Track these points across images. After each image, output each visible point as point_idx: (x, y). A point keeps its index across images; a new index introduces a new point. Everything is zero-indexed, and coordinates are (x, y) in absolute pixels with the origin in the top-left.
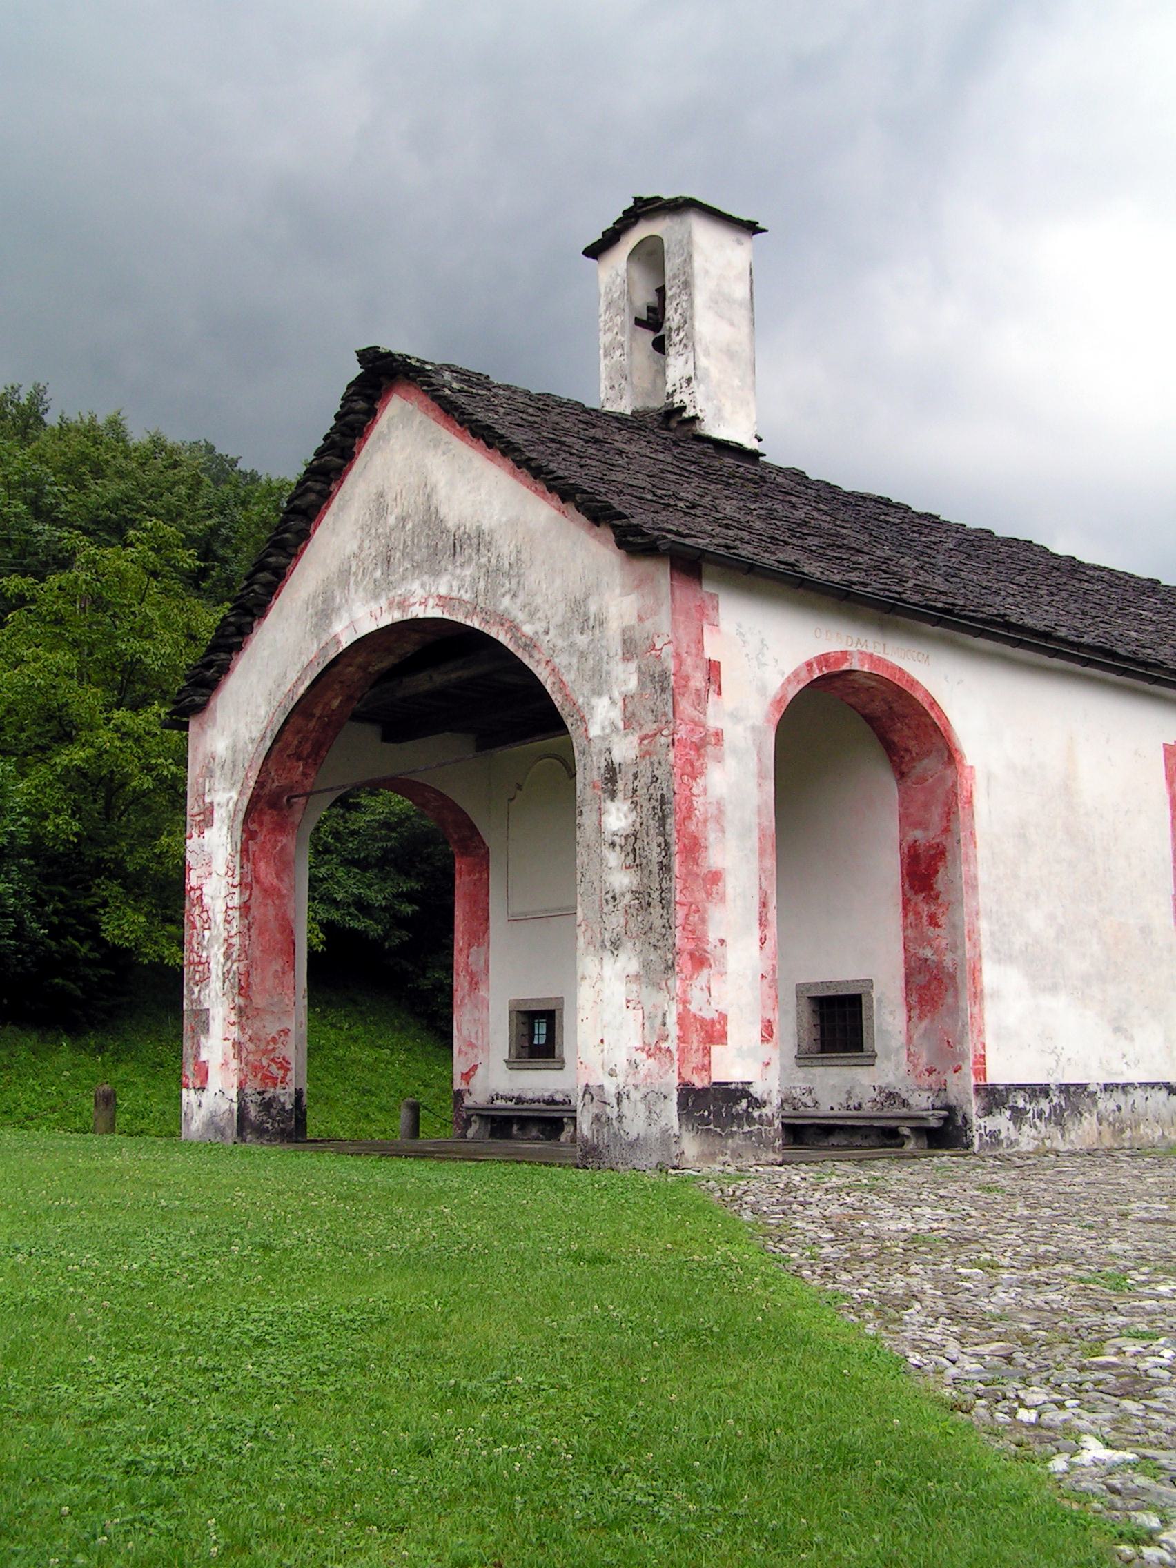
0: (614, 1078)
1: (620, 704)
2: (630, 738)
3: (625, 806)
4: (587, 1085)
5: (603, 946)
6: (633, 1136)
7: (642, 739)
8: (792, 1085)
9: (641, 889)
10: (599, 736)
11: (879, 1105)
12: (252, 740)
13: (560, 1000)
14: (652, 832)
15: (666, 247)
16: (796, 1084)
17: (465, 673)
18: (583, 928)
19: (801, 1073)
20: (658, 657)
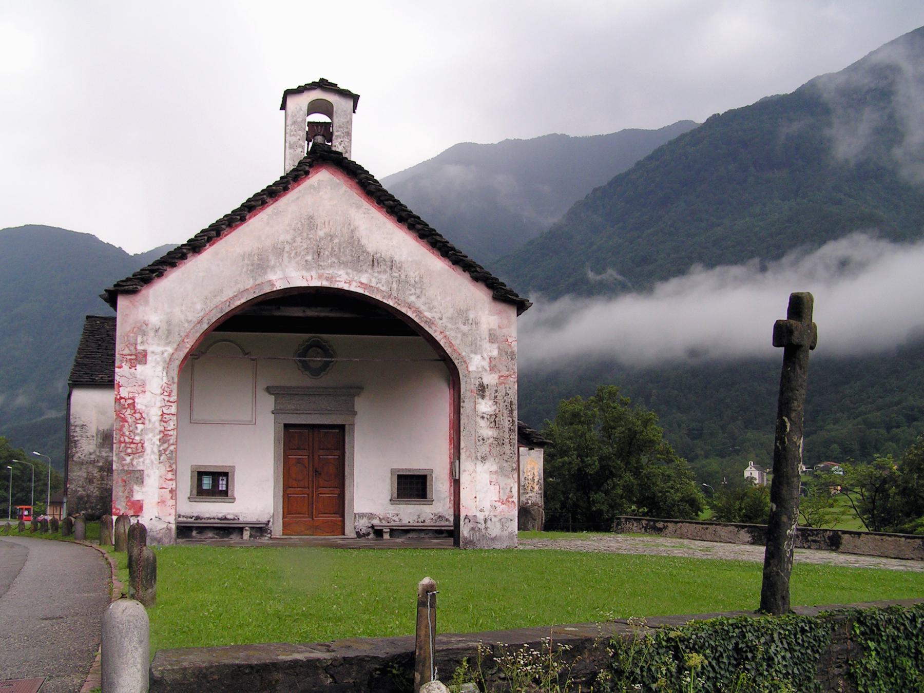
0: (483, 513)
1: (488, 360)
2: (493, 375)
3: (491, 403)
5: (477, 458)
6: (493, 535)
7: (500, 377)
10: (475, 371)
12: (189, 322)
13: (233, 467)
14: (505, 415)
15: (335, 109)
17: (322, 314)
18: (464, 450)
19: (392, 507)
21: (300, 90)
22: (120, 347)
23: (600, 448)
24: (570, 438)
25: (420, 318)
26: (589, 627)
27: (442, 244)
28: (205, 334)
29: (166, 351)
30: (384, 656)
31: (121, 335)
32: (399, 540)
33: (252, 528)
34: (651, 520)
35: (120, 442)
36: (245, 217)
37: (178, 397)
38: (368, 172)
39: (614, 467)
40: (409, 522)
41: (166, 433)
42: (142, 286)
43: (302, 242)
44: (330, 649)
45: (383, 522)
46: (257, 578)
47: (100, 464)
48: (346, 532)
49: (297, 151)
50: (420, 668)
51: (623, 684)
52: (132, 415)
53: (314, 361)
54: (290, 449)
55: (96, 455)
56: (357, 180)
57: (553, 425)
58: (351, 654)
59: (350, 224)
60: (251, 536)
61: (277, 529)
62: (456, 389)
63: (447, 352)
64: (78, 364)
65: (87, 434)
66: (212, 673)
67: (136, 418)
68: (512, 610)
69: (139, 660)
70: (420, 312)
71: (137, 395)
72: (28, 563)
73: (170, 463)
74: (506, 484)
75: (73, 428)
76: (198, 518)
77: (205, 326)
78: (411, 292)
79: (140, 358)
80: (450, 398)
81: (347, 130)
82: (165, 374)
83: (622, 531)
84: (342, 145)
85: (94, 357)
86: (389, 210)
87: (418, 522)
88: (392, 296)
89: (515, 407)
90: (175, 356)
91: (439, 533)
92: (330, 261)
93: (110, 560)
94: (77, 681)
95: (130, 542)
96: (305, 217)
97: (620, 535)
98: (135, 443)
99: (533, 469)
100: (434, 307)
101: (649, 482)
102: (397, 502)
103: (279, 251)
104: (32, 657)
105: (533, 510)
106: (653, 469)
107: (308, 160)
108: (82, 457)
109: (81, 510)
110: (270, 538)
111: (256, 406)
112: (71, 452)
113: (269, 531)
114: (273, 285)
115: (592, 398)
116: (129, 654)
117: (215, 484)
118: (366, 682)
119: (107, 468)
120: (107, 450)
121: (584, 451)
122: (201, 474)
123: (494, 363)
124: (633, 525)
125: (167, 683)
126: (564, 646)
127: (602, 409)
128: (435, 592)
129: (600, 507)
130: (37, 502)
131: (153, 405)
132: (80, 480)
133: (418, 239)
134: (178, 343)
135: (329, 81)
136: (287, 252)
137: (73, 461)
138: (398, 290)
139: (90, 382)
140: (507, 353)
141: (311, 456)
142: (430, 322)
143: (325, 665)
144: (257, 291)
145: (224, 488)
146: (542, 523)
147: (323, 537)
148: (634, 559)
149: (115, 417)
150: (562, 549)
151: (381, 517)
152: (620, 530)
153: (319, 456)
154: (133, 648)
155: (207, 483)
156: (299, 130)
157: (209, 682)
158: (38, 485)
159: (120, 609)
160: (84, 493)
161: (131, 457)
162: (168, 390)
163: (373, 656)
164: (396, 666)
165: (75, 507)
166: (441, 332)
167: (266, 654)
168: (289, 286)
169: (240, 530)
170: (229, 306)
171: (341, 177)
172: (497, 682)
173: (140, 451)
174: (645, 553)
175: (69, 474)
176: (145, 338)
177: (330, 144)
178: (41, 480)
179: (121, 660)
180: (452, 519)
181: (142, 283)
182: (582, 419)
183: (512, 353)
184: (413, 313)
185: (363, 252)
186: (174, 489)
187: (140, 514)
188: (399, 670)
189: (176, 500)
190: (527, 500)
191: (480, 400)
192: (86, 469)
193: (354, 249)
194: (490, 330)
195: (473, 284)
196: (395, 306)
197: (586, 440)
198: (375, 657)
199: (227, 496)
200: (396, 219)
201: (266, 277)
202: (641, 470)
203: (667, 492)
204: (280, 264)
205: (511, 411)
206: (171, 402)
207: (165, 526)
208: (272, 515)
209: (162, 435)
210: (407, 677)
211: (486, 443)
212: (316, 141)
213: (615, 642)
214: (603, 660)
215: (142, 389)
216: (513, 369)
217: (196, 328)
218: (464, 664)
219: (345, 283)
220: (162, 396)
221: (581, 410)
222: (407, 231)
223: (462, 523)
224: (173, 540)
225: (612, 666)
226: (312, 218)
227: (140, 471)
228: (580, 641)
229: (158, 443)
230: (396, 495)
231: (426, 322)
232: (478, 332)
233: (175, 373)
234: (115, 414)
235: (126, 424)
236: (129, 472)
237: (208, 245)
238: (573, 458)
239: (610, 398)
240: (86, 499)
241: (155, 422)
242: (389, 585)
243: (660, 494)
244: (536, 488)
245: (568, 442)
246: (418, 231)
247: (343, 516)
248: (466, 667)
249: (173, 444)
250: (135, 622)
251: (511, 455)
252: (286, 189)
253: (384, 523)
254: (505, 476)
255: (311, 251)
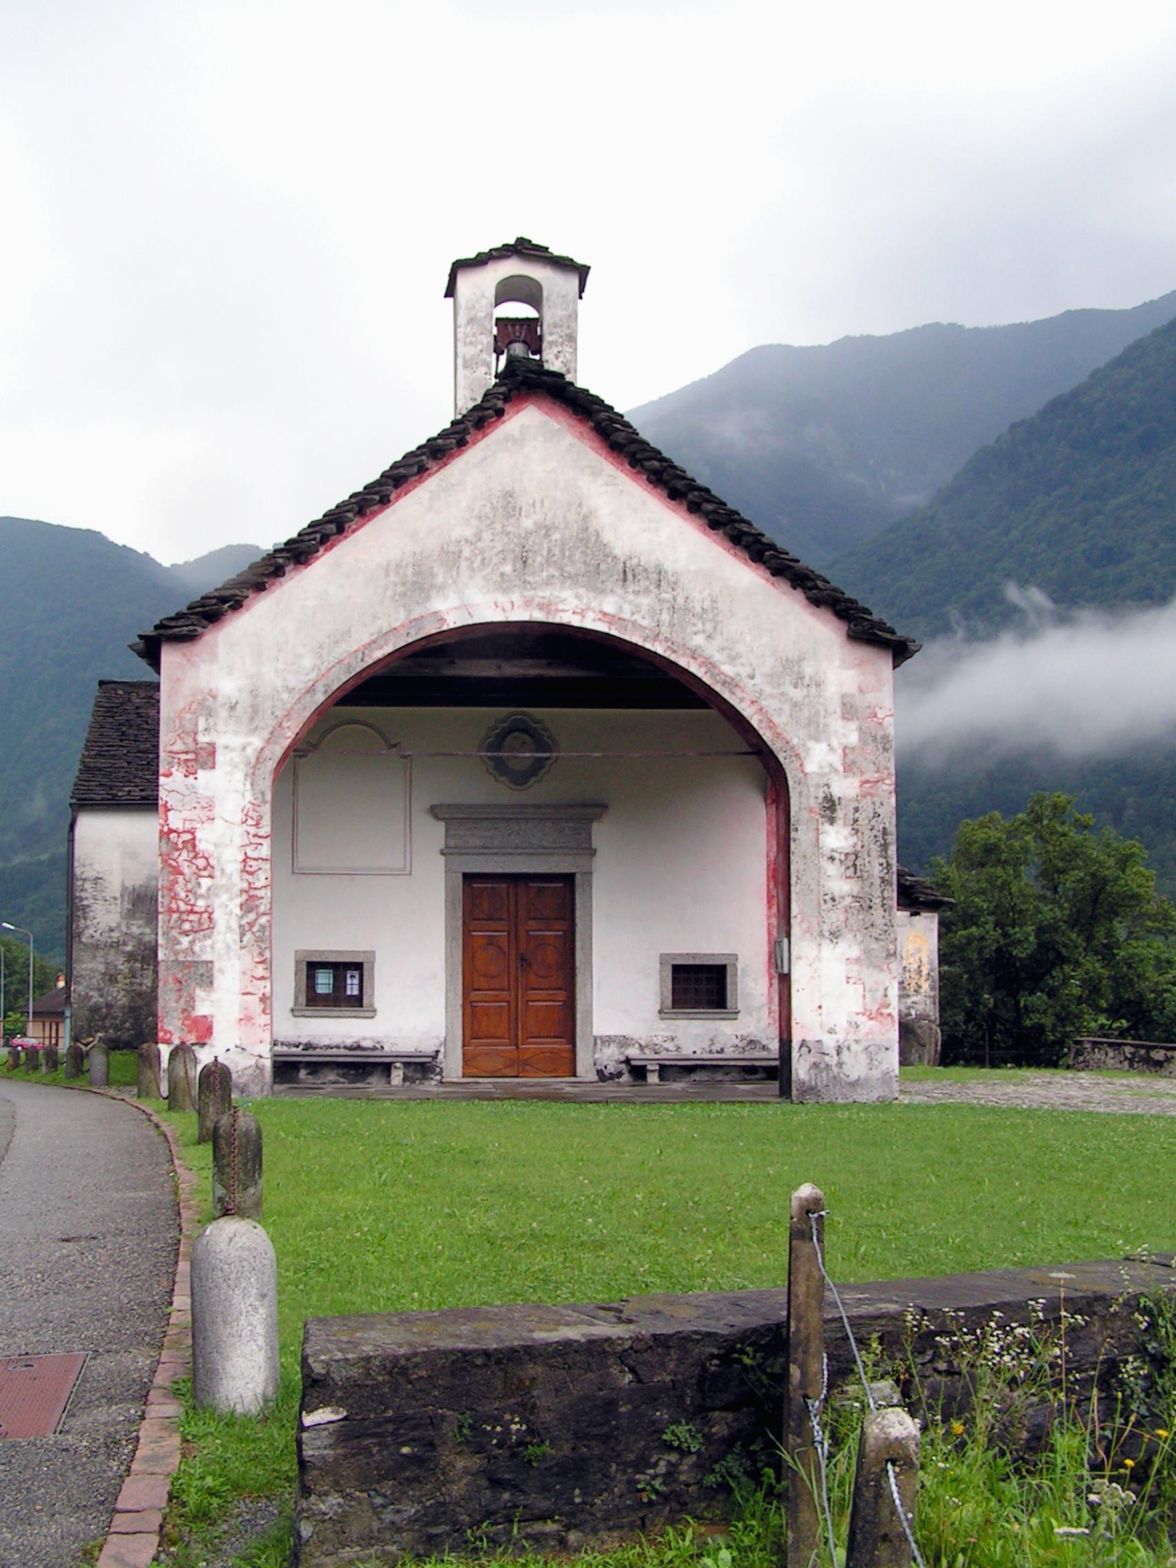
0: (833, 1036)
1: (840, 752)
2: (850, 780)
4: (804, 1041)
5: (821, 935)
8: (653, 1034)
9: (862, 895)
11: (741, 1050)
12: (290, 690)
13: (372, 953)
14: (873, 854)
15: (545, 293)
16: (658, 1033)
17: (533, 672)
18: (799, 919)
19: (663, 1024)
20: (880, 724)
21: (481, 261)
22: (166, 739)
23: (1038, 911)
24: (982, 892)
25: (713, 676)
26: (1094, 1272)
27: (751, 539)
28: (320, 712)
29: (250, 744)
30: (726, 1333)
31: (169, 717)
32: (677, 1086)
33: (406, 1065)
34: (1142, 1047)
35: (171, 911)
36: (388, 496)
37: (272, 828)
38: (612, 408)
39: (1065, 946)
40: (695, 1052)
41: (252, 893)
42: (204, 627)
43: (492, 540)
44: (624, 1316)
45: (647, 1051)
46: (438, 1163)
47: (129, 948)
48: (580, 1069)
49: (478, 373)
50: (799, 1355)
51: (1168, 1384)
52: (190, 862)
53: (516, 757)
54: (475, 919)
55: (120, 931)
56: (591, 424)
57: (951, 871)
58: (664, 1328)
59: (580, 505)
60: (405, 1079)
61: (453, 1066)
62: (782, 806)
63: (764, 737)
64: (86, 769)
65: (104, 894)
66: (417, 1365)
67: (197, 867)
68: (917, 1226)
69: (260, 1330)
70: (714, 666)
71: (198, 826)
72: (18, 1132)
73: (260, 947)
74: (876, 983)
75: (79, 883)
76: (308, 1046)
77: (320, 698)
78: (695, 629)
79: (204, 757)
80: (769, 823)
81: (568, 331)
82: (248, 786)
83: (1086, 1066)
84: (561, 359)
85: (115, 755)
86: (654, 478)
87: (711, 1052)
88: (661, 637)
89: (892, 838)
90: (267, 753)
91: (749, 1071)
92: (545, 574)
93: (165, 1127)
94: (144, 1362)
95: (203, 1097)
96: (499, 494)
97: (1082, 1074)
98: (196, 913)
99: (919, 950)
100: (738, 656)
101: (1132, 971)
102: (672, 1016)
103: (451, 557)
104: (56, 1313)
105: (920, 1027)
106: (1139, 948)
107: (503, 389)
108: (97, 935)
109: (97, 1031)
110: (441, 1082)
111: (411, 842)
112: (78, 927)
113: (438, 1070)
114: (442, 620)
115: (1020, 816)
116: (242, 1318)
117: (339, 984)
118: (694, 1381)
119: (147, 955)
120: (141, 922)
121: (1007, 916)
122: (313, 967)
123: (851, 757)
124: (1107, 1054)
125: (337, 1384)
126: (1073, 1318)
127: (1039, 837)
128: (823, 1213)
129: (1040, 1019)
130: (10, 1013)
131: (228, 842)
132: (93, 978)
133: (707, 528)
134: (270, 729)
135: (534, 242)
136: (467, 559)
137: (81, 942)
138: (672, 625)
139: (109, 800)
140: (874, 738)
141: (513, 933)
142: (732, 683)
143: (619, 1349)
144: (413, 632)
145: (356, 992)
146: (936, 1051)
147: (536, 1080)
148: (1124, 1124)
149: (160, 866)
150: (982, 1102)
151: (643, 1043)
152: (1082, 1065)
153: (528, 931)
154: (250, 1308)
155: (324, 981)
156: (481, 334)
157: (410, 1382)
158: (12, 983)
159: (225, 1237)
160: (101, 1000)
161: (190, 938)
162: (254, 815)
163: (707, 1332)
164: (749, 1349)
165: (86, 1026)
166: (753, 702)
167: (508, 1327)
168: (470, 622)
169: (386, 1068)
170: (362, 660)
171: (561, 418)
172: (932, 1379)
173: (205, 926)
174: (1139, 1111)
175: (74, 966)
176: (211, 721)
177: (537, 357)
178: (15, 972)
179: (229, 1330)
180: (775, 1045)
181: (204, 622)
182: (1004, 856)
183: (886, 738)
184: (700, 666)
185: (607, 556)
186: (268, 995)
187: (207, 1041)
188: (754, 1358)
189: (271, 1014)
190: (909, 1008)
191: (827, 827)
192: (103, 957)
193: (589, 551)
194: (843, 696)
195: (809, 610)
196: (667, 654)
197: (1010, 894)
198: (709, 1334)
199: (362, 1006)
200: (665, 493)
201: (428, 605)
202: (1116, 951)
203: (1166, 991)
204: (454, 582)
205: (885, 847)
206: (261, 837)
207: (252, 1062)
208: (442, 1039)
209: (245, 897)
210: (769, 1370)
211: (839, 906)
212: (512, 352)
213: (1151, 1304)
214: (1127, 1337)
215: (208, 813)
216: (887, 768)
217: (303, 702)
218: (875, 1345)
219: (574, 613)
220: (245, 827)
221: (1000, 839)
222: (687, 515)
223: (795, 1054)
224: (266, 1088)
225: (1146, 1349)
226: (510, 496)
227: (207, 962)
228: (1084, 1301)
229: (238, 911)
230: (669, 1002)
231: (724, 683)
232: (821, 700)
233: (266, 784)
234: (160, 860)
235: (180, 878)
236: (187, 965)
237: (322, 549)
238: (988, 930)
239: (1055, 816)
240: (104, 1011)
241: (232, 874)
242: (681, 1178)
243: (1153, 995)
244: (926, 986)
245: (976, 900)
246: (706, 515)
247: (573, 1042)
248: (878, 1352)
249: (264, 914)
250: (252, 1260)
251: (886, 928)
252: (462, 444)
253: (649, 1054)
254: (875, 967)
255: (510, 556)
